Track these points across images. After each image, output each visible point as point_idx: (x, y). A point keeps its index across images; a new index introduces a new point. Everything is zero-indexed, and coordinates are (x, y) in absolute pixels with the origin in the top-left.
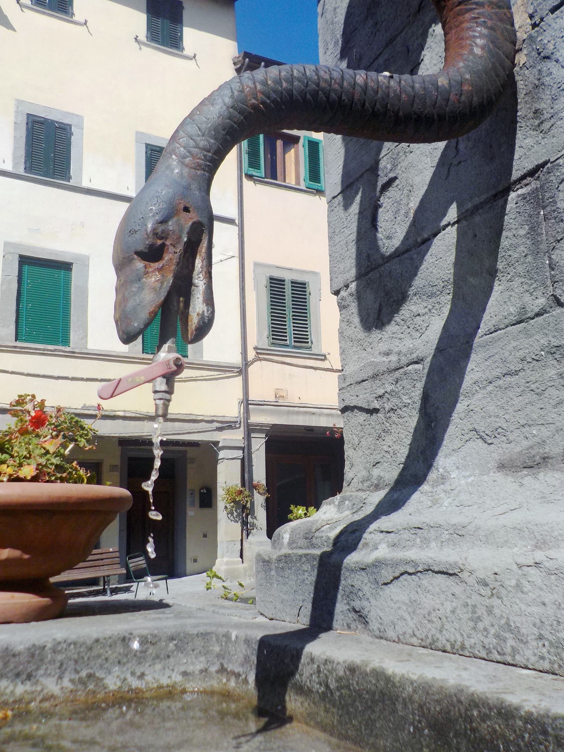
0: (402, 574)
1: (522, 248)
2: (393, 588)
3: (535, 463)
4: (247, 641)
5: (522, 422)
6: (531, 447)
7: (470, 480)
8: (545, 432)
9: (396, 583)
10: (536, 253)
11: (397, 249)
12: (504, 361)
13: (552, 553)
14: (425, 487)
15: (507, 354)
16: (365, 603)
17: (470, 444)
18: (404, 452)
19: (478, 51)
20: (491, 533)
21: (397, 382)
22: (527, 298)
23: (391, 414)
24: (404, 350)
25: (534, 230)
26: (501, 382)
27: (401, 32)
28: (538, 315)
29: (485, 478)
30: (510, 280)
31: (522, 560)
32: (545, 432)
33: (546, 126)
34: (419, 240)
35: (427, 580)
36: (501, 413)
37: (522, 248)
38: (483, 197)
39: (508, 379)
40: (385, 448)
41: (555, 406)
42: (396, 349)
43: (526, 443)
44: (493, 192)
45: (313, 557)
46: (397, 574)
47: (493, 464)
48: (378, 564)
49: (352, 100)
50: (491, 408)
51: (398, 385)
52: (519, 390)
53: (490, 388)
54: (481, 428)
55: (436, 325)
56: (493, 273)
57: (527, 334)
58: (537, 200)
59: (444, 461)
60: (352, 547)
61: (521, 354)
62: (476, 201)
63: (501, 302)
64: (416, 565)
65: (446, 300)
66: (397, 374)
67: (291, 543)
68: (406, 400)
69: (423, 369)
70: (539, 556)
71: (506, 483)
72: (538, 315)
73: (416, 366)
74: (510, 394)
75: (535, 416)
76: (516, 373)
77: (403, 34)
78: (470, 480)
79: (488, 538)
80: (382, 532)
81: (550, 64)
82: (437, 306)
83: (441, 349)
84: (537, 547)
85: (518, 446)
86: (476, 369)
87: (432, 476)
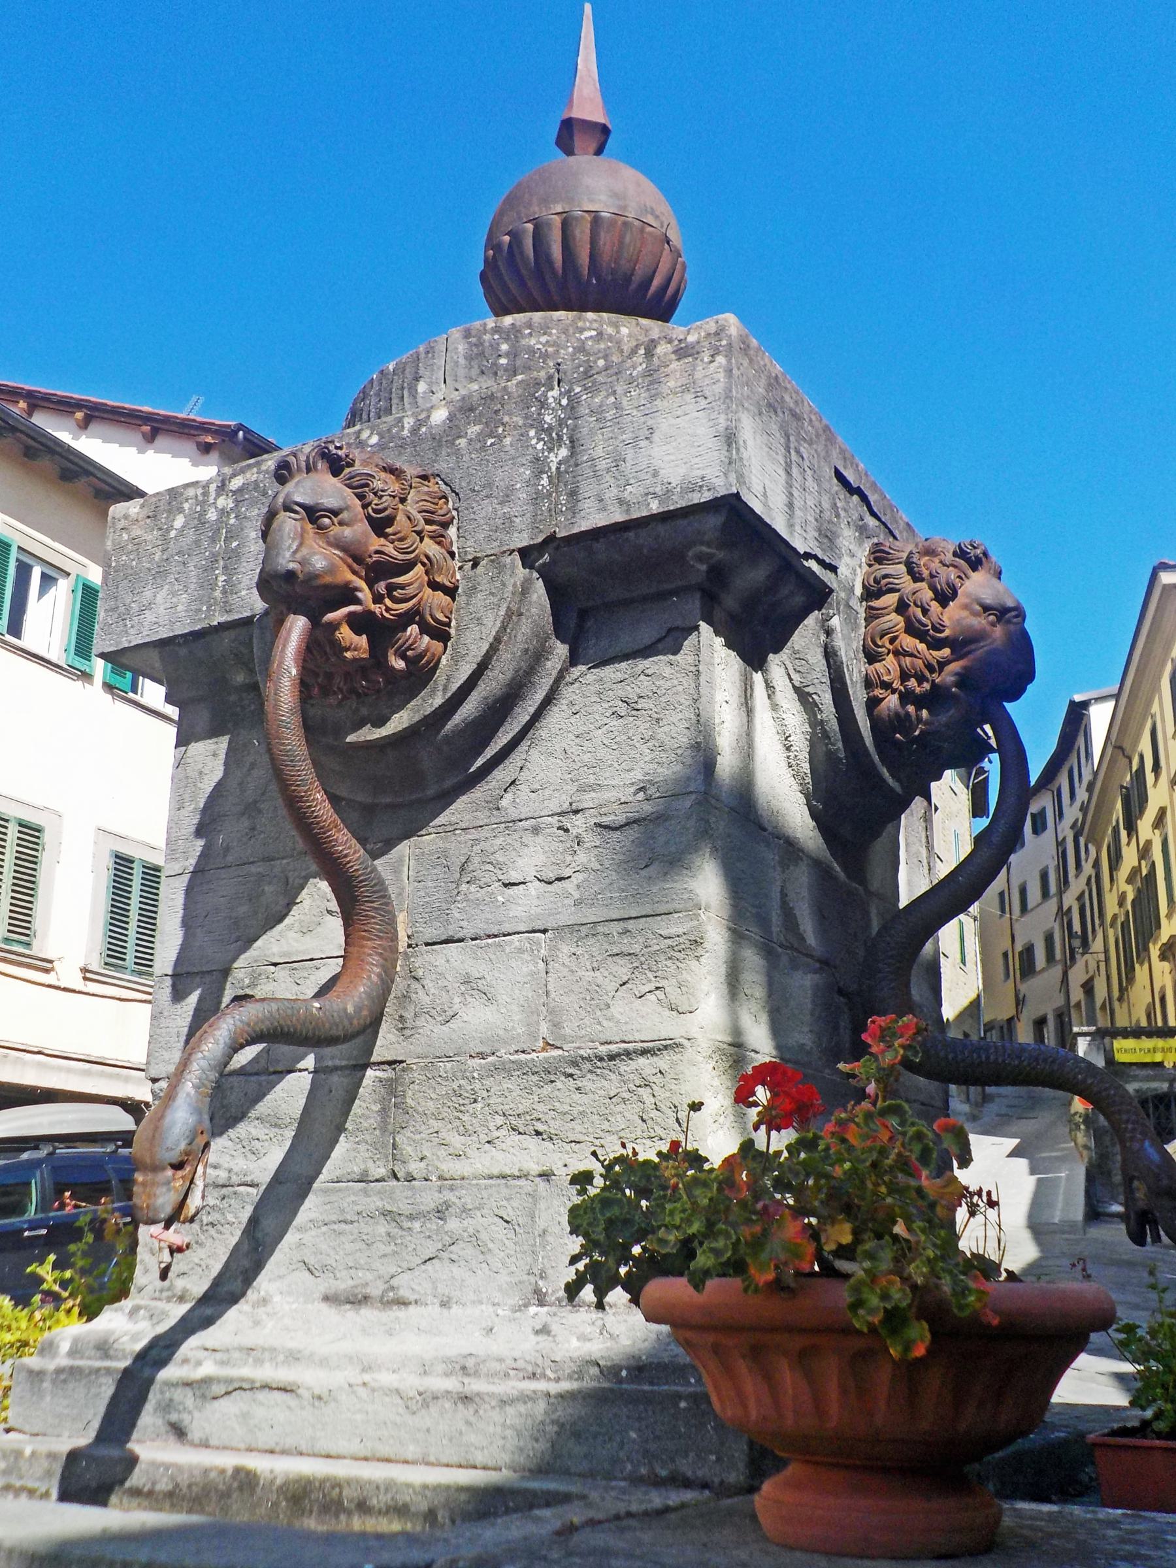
0: (236, 1390)
1: (372, 1121)
2: (223, 1402)
3: (357, 1300)
4: (52, 1456)
5: (350, 1264)
6: (356, 1287)
7: (294, 1306)
8: (369, 1276)
9: (226, 1398)
10: (384, 1130)
11: (242, 1067)
12: (343, 1211)
13: (377, 1376)
14: (243, 1306)
15: (345, 1205)
16: (186, 1417)
17: (297, 1273)
18: (216, 1268)
19: (374, 978)
20: (326, 1359)
21: (223, 1198)
22: (370, 1164)
23: (210, 1228)
24: (236, 1169)
25: (384, 1111)
26: (336, 1227)
27: (283, 858)
28: (377, 1181)
29: (310, 1306)
30: (358, 1143)
31: (352, 1381)
32: (369, 1276)
33: (407, 1032)
34: (271, 1070)
35: (262, 1396)
36: (332, 1253)
37: (372, 1121)
38: (344, 1063)
39: (343, 1226)
40: (197, 1260)
41: (380, 1257)
42: (226, 1165)
43: (350, 1283)
44: (352, 1062)
45: (116, 1370)
46: (230, 1389)
47: (318, 1295)
48: (207, 1381)
49: (295, 1032)
50: (324, 1247)
51: (224, 1202)
52: (352, 1238)
53: (324, 1229)
54: (311, 1261)
55: (275, 1156)
56: (340, 1129)
57: (366, 1193)
58: (392, 1088)
59: (264, 1283)
60: (163, 1363)
61: (359, 1208)
62: (337, 1062)
63: (344, 1156)
64: (253, 1382)
65: (290, 1133)
66: (225, 1191)
67: (73, 1352)
68: (230, 1217)
69: (255, 1194)
70: (367, 1377)
71: (329, 1313)
72: (377, 1181)
73: (250, 1189)
74: (343, 1238)
75: (362, 1262)
76: (352, 1222)
77: (285, 861)
78: (294, 1306)
79: (323, 1362)
80: (207, 1349)
81: (415, 985)
82: (279, 1137)
83: (278, 1178)
84: (364, 1370)
85: (343, 1284)
86: (311, 1208)
87: (251, 1295)
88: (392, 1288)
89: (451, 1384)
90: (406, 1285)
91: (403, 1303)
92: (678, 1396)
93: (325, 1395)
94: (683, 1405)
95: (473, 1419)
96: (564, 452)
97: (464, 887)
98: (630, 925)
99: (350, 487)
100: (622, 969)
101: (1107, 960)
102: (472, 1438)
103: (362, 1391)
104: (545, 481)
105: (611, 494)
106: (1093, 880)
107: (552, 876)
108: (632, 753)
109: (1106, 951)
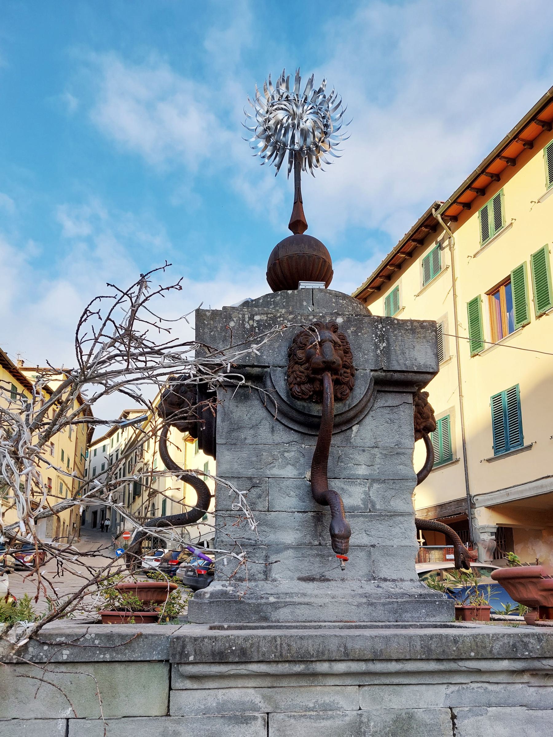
85: (305, 575)
88: (323, 576)
89: (364, 600)
90: (328, 574)
91: (328, 580)
92: (436, 601)
93: (323, 605)
94: (437, 603)
95: (374, 609)
96: (384, 345)
97: (339, 463)
98: (396, 481)
99: (339, 338)
100: (393, 492)
101: (124, 495)
102: (374, 614)
103: (336, 604)
104: (379, 351)
105: (401, 361)
106: (122, 469)
107: (370, 464)
108: (393, 434)
109: (124, 492)
